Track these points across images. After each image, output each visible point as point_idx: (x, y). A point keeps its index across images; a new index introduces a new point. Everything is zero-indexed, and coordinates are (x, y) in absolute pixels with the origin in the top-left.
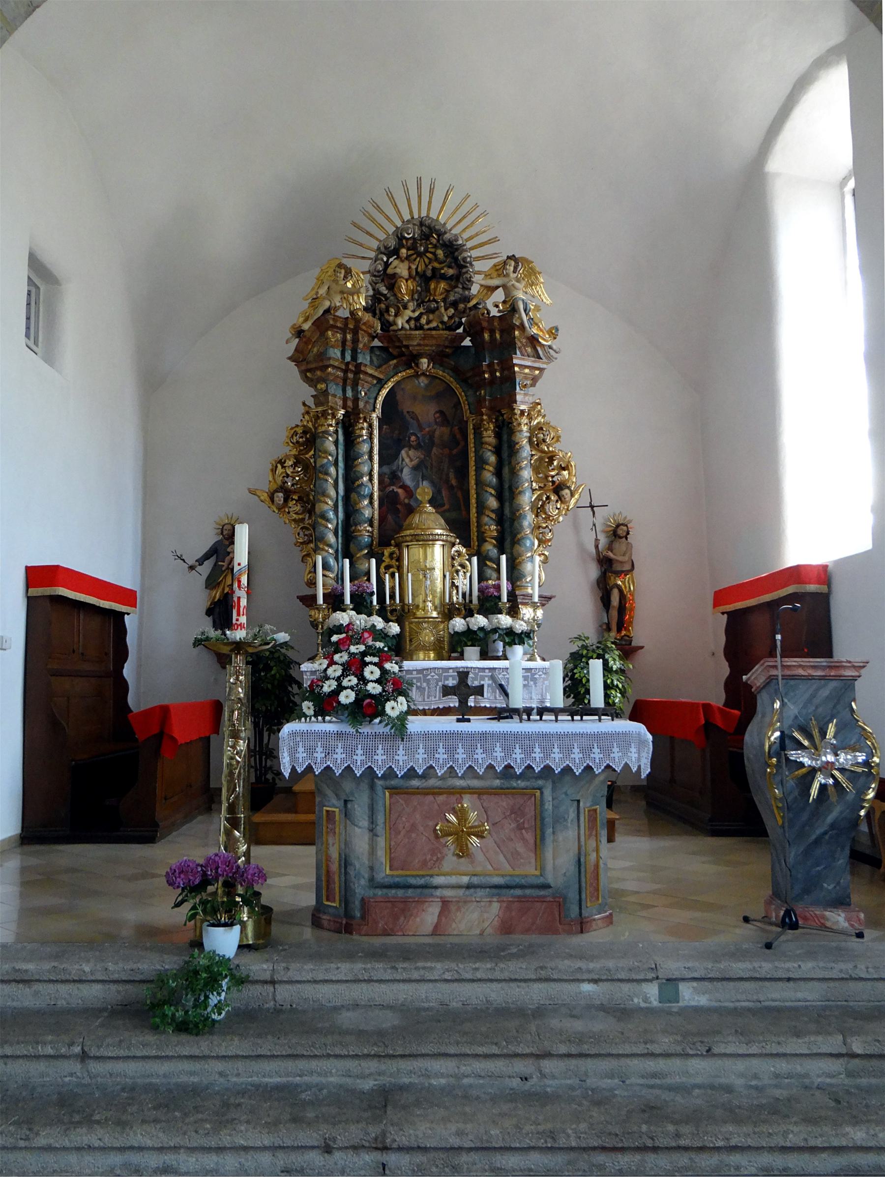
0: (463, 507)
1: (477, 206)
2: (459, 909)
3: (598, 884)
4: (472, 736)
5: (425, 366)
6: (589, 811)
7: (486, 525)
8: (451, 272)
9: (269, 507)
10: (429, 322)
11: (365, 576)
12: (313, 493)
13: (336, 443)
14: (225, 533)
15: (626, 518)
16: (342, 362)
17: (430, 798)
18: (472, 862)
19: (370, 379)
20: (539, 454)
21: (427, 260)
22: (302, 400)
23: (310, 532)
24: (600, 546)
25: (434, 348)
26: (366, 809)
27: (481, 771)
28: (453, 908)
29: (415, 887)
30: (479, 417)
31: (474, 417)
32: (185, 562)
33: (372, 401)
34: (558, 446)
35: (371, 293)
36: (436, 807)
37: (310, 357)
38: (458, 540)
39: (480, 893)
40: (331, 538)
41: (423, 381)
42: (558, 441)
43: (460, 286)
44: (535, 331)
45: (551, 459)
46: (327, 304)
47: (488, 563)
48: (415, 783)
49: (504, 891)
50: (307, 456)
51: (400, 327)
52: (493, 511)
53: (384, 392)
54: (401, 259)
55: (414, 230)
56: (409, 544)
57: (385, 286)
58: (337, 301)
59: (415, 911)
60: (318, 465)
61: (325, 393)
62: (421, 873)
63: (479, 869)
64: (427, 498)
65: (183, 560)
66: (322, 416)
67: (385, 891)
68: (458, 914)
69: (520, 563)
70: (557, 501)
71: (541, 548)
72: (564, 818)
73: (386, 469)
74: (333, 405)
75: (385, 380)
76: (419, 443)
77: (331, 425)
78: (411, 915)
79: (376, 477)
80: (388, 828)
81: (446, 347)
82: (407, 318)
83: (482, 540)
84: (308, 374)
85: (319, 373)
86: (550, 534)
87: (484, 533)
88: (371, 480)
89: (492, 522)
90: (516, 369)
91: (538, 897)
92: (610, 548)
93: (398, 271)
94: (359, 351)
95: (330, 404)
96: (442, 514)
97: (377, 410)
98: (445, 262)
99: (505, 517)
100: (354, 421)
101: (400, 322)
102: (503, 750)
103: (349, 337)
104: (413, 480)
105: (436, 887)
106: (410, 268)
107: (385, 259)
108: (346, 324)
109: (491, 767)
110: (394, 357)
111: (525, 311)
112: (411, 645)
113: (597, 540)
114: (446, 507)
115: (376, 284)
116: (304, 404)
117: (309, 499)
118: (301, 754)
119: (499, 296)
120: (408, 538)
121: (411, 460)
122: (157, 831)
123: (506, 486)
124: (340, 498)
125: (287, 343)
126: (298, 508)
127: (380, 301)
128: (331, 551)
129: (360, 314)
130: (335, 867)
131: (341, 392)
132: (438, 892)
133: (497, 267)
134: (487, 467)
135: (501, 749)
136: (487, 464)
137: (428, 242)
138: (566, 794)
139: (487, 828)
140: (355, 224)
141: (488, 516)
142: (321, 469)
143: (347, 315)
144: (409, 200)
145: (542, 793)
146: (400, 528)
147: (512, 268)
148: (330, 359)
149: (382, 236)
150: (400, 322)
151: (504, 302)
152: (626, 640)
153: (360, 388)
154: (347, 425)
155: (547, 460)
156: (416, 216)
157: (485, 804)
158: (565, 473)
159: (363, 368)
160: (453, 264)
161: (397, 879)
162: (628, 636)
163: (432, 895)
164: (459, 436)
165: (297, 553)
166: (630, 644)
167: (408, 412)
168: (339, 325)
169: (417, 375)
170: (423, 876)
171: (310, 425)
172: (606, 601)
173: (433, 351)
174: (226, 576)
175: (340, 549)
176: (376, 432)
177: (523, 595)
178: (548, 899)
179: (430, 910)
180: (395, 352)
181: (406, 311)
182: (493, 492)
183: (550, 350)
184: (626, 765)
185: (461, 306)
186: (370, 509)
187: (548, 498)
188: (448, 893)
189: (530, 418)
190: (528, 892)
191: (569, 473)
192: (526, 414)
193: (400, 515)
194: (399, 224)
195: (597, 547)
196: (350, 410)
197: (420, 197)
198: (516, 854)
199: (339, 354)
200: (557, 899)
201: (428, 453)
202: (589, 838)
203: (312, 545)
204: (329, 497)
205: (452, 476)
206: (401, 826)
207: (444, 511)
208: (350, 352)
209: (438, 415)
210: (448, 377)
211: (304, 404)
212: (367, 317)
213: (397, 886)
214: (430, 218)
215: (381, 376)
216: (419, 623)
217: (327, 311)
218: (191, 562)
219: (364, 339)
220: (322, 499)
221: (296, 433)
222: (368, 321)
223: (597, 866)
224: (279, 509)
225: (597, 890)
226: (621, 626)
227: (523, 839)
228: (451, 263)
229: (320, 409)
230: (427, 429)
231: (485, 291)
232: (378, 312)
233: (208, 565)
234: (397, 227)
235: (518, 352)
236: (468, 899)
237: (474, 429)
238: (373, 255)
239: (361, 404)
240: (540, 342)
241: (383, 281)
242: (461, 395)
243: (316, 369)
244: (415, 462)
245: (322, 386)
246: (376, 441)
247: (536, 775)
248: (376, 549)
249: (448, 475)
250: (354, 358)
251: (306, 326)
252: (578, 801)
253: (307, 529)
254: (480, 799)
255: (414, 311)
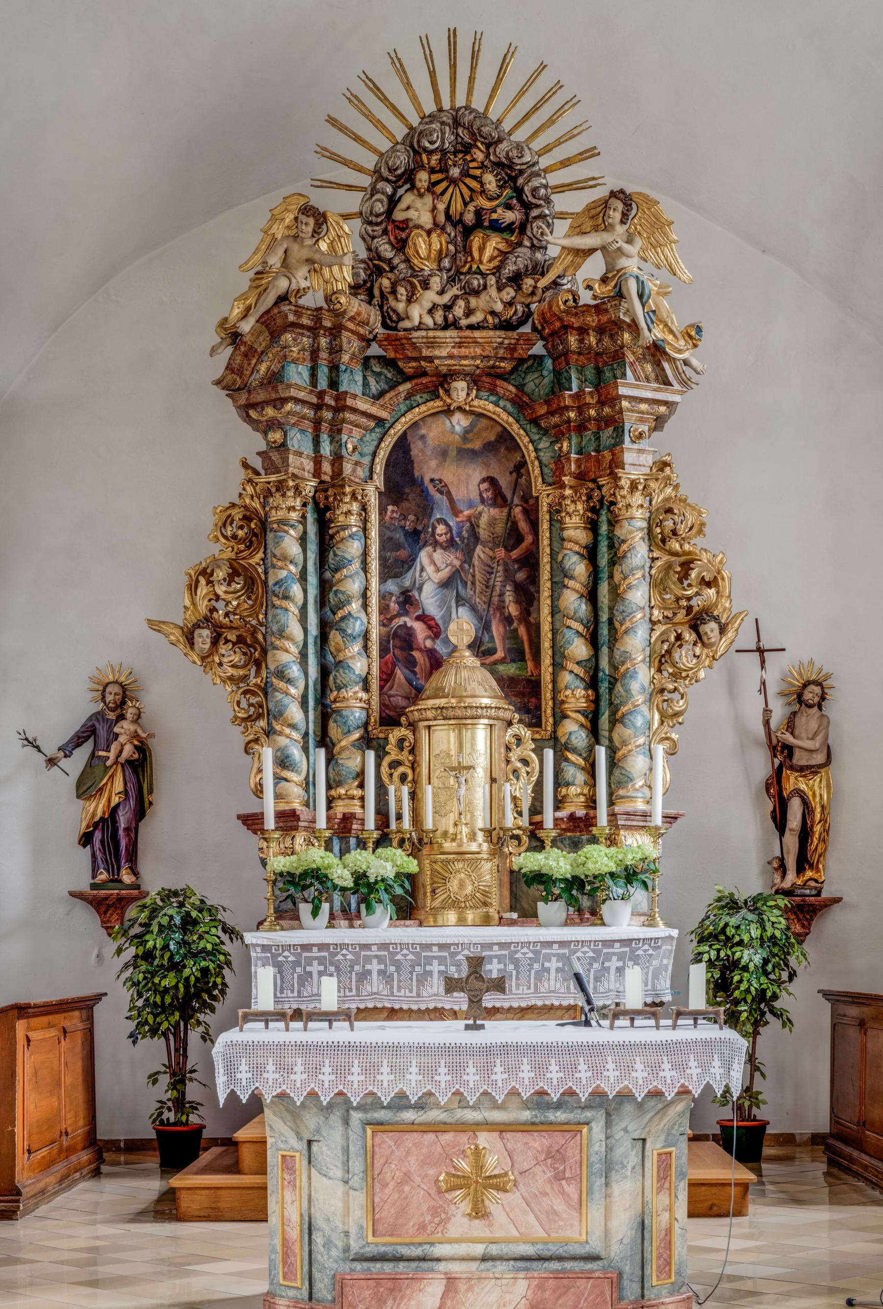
0: (528, 655)
1: (559, 86)
2: (470, 1289)
3: (670, 1257)
4: (488, 1050)
5: (463, 395)
6: (659, 1154)
7: (566, 688)
8: (510, 216)
9: (186, 655)
10: (469, 313)
11: (355, 778)
12: (263, 629)
13: (303, 540)
14: (109, 698)
15: (821, 670)
16: (311, 392)
17: (431, 1137)
18: (490, 1225)
19: (364, 421)
20: (666, 558)
21: (467, 193)
22: (240, 456)
23: (258, 699)
24: (773, 724)
25: (478, 362)
26: (339, 1152)
27: (500, 1098)
28: (462, 1286)
29: (410, 1260)
30: (558, 492)
31: (550, 490)
32: (40, 751)
33: (366, 460)
34: (699, 541)
35: (363, 255)
36: (439, 1149)
37: (254, 380)
38: (517, 716)
39: (501, 1267)
40: (295, 712)
41: (460, 422)
42: (700, 532)
43: (527, 243)
44: (658, 333)
45: (687, 566)
46: (283, 284)
47: (570, 756)
48: (409, 1115)
49: (535, 1264)
50: (251, 561)
51: (417, 323)
52: (578, 663)
53: (389, 442)
54: (418, 191)
55: (443, 134)
56: (431, 723)
57: (390, 243)
58: (301, 278)
59: (408, 1292)
60: (271, 582)
61: (282, 447)
62: (416, 1240)
63: (499, 1234)
64: (467, 640)
65: (38, 748)
66: (278, 490)
67: (366, 1265)
68: (470, 1294)
69: (625, 756)
70: (695, 644)
71: (666, 728)
72: (622, 1163)
73: (392, 586)
74: (296, 471)
75: (392, 420)
76: (452, 538)
77: (291, 509)
78: (402, 1297)
79: (374, 601)
80: (369, 1179)
81: (503, 359)
82: (430, 305)
83: (560, 716)
84: (252, 413)
85: (270, 412)
86: (681, 702)
87: (563, 702)
88: (365, 606)
89: (578, 683)
90: (625, 404)
91: (582, 1272)
92: (790, 725)
93: (412, 214)
94: (343, 368)
95: (291, 470)
96: (491, 668)
97: (375, 477)
98: (499, 196)
99: (601, 674)
100: (335, 499)
101: (417, 313)
102: (533, 1068)
103: (324, 342)
104: (440, 607)
105: (438, 1260)
106: (434, 209)
107: (389, 190)
108: (318, 320)
109: (514, 1093)
110: (408, 378)
111: (641, 296)
112: (433, 900)
113: (767, 711)
114: (500, 654)
115: (373, 238)
116: (245, 465)
117: (256, 641)
118: (244, 1074)
119: (594, 267)
120: (429, 714)
121: (438, 570)
122: (18, 1201)
123: (604, 617)
124: (311, 641)
125: (211, 355)
126: (237, 658)
127: (380, 272)
128: (296, 735)
129: (343, 300)
130: (294, 1234)
131: (310, 445)
132: (442, 1266)
133: (593, 212)
134: (571, 583)
135: (557, 1068)
136: (571, 578)
137: (468, 158)
138: (626, 1130)
139: (512, 1178)
140: (333, 121)
141: (571, 672)
142: (276, 588)
143: (321, 303)
144: (433, 74)
145: (590, 1130)
146: (416, 694)
147: (618, 216)
148: (289, 386)
149: (384, 145)
150: (417, 313)
151: (604, 280)
152: (811, 888)
153: (344, 437)
154: (322, 506)
155: (679, 569)
156: (446, 105)
157: (509, 1146)
158: (712, 592)
159: (349, 402)
160: (515, 201)
161: (383, 1249)
162: (816, 881)
163: (432, 1270)
164: (523, 526)
165: (237, 736)
166: (819, 894)
167: (432, 480)
168: (305, 321)
169: (448, 412)
170: (420, 1244)
171: (256, 504)
172: (780, 820)
173: (477, 367)
174: (112, 776)
175: (311, 732)
176: (374, 517)
177: (628, 814)
178: (597, 1275)
179: (430, 1289)
180: (409, 368)
181: (428, 292)
182: (581, 628)
183: (685, 368)
184: (708, 1086)
185: (528, 282)
186: (364, 661)
187: (679, 637)
188: (455, 1268)
189: (647, 493)
190: (568, 1265)
191: (718, 592)
192: (640, 487)
193: (417, 669)
194: (415, 120)
195: (767, 723)
196: (327, 478)
197: (453, 67)
198: (552, 1213)
199: (306, 375)
200: (609, 1275)
201: (468, 554)
202: (658, 1193)
203: (263, 723)
204: (289, 638)
205: (509, 597)
206: (388, 1176)
207: (495, 663)
208: (326, 370)
209: (485, 485)
210: (504, 416)
211: (245, 465)
212: (355, 306)
213: (382, 1258)
214: (473, 111)
215: (384, 414)
216: (448, 861)
217: (283, 298)
218: (51, 749)
219: (351, 345)
220: (278, 642)
221: (229, 520)
222: (358, 314)
223: (669, 1231)
224: (203, 659)
225: (669, 1264)
226: (803, 862)
227: (563, 1192)
228: (511, 198)
229: (273, 478)
230: (466, 513)
231: (570, 258)
232: (376, 292)
233: (82, 754)
234: (411, 128)
235: (629, 373)
236: (484, 1275)
237: (550, 512)
238: (366, 181)
239: (348, 468)
240: (665, 353)
241: (385, 232)
242: (527, 448)
243: (267, 403)
244: (445, 573)
245: (276, 436)
246: (374, 533)
247: (583, 1105)
248: (377, 732)
249: (501, 595)
250: (334, 384)
251: (246, 327)
252: (644, 1140)
253: (254, 694)
254: (502, 1138)
255: (441, 293)
